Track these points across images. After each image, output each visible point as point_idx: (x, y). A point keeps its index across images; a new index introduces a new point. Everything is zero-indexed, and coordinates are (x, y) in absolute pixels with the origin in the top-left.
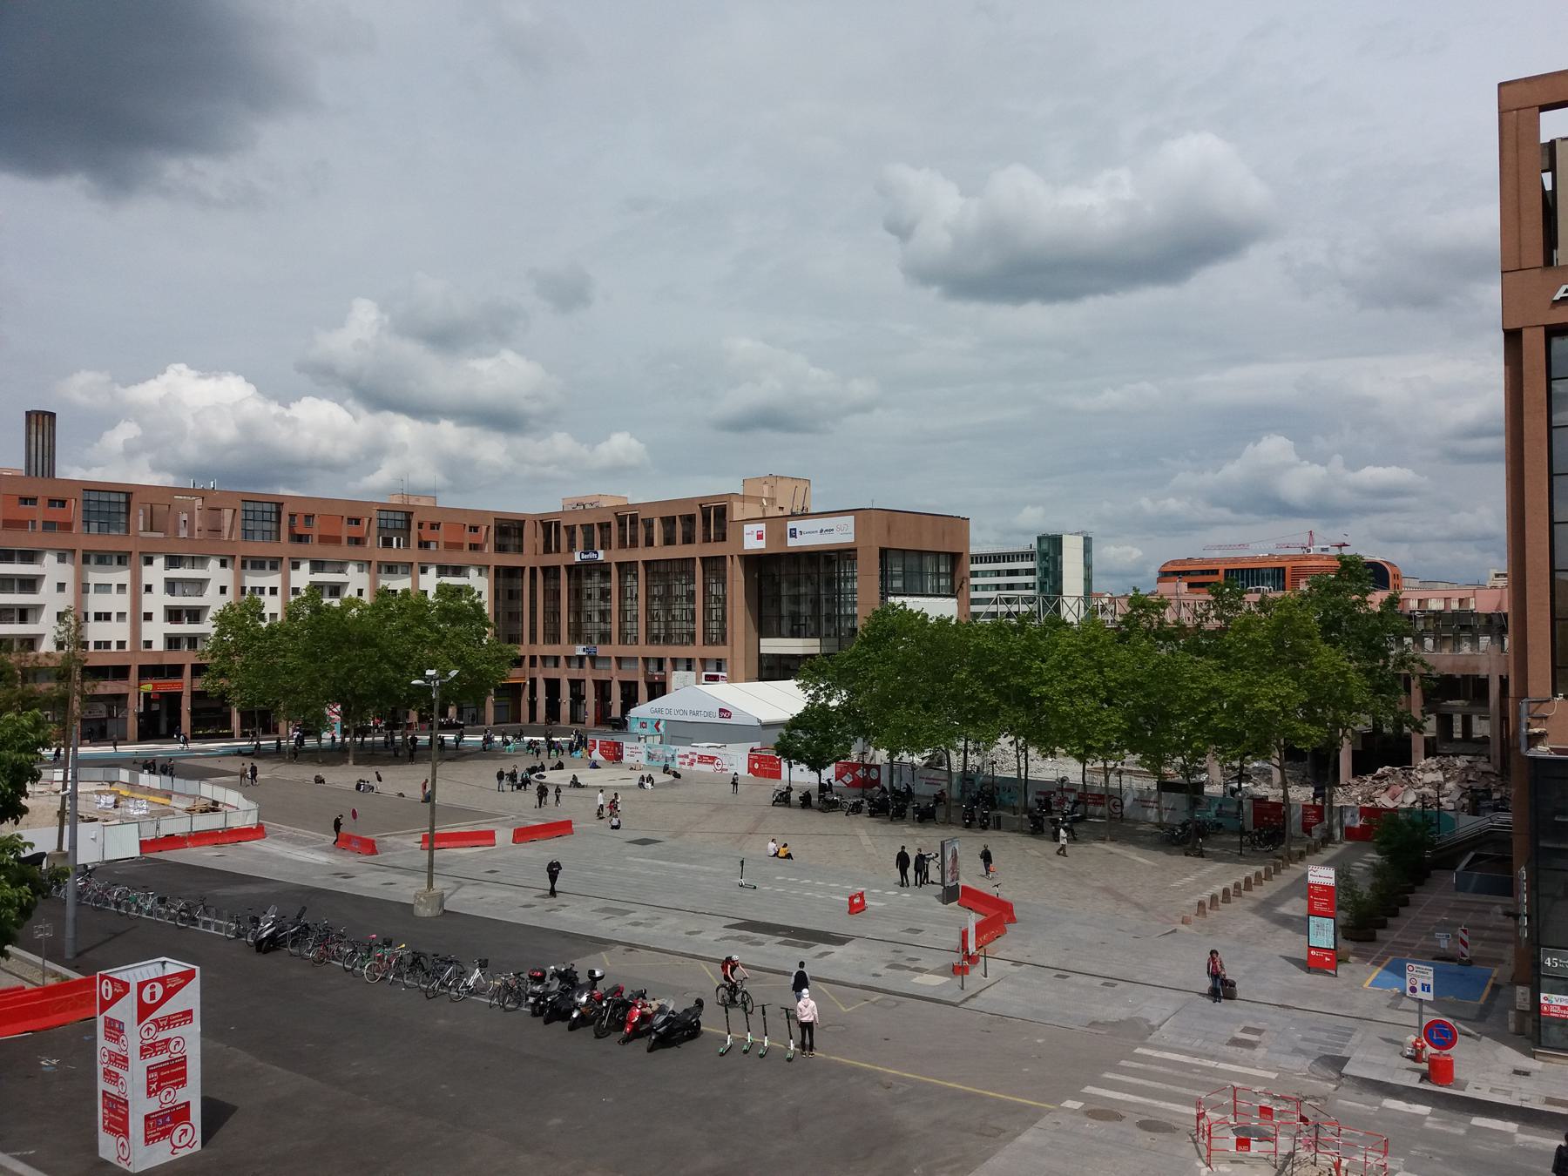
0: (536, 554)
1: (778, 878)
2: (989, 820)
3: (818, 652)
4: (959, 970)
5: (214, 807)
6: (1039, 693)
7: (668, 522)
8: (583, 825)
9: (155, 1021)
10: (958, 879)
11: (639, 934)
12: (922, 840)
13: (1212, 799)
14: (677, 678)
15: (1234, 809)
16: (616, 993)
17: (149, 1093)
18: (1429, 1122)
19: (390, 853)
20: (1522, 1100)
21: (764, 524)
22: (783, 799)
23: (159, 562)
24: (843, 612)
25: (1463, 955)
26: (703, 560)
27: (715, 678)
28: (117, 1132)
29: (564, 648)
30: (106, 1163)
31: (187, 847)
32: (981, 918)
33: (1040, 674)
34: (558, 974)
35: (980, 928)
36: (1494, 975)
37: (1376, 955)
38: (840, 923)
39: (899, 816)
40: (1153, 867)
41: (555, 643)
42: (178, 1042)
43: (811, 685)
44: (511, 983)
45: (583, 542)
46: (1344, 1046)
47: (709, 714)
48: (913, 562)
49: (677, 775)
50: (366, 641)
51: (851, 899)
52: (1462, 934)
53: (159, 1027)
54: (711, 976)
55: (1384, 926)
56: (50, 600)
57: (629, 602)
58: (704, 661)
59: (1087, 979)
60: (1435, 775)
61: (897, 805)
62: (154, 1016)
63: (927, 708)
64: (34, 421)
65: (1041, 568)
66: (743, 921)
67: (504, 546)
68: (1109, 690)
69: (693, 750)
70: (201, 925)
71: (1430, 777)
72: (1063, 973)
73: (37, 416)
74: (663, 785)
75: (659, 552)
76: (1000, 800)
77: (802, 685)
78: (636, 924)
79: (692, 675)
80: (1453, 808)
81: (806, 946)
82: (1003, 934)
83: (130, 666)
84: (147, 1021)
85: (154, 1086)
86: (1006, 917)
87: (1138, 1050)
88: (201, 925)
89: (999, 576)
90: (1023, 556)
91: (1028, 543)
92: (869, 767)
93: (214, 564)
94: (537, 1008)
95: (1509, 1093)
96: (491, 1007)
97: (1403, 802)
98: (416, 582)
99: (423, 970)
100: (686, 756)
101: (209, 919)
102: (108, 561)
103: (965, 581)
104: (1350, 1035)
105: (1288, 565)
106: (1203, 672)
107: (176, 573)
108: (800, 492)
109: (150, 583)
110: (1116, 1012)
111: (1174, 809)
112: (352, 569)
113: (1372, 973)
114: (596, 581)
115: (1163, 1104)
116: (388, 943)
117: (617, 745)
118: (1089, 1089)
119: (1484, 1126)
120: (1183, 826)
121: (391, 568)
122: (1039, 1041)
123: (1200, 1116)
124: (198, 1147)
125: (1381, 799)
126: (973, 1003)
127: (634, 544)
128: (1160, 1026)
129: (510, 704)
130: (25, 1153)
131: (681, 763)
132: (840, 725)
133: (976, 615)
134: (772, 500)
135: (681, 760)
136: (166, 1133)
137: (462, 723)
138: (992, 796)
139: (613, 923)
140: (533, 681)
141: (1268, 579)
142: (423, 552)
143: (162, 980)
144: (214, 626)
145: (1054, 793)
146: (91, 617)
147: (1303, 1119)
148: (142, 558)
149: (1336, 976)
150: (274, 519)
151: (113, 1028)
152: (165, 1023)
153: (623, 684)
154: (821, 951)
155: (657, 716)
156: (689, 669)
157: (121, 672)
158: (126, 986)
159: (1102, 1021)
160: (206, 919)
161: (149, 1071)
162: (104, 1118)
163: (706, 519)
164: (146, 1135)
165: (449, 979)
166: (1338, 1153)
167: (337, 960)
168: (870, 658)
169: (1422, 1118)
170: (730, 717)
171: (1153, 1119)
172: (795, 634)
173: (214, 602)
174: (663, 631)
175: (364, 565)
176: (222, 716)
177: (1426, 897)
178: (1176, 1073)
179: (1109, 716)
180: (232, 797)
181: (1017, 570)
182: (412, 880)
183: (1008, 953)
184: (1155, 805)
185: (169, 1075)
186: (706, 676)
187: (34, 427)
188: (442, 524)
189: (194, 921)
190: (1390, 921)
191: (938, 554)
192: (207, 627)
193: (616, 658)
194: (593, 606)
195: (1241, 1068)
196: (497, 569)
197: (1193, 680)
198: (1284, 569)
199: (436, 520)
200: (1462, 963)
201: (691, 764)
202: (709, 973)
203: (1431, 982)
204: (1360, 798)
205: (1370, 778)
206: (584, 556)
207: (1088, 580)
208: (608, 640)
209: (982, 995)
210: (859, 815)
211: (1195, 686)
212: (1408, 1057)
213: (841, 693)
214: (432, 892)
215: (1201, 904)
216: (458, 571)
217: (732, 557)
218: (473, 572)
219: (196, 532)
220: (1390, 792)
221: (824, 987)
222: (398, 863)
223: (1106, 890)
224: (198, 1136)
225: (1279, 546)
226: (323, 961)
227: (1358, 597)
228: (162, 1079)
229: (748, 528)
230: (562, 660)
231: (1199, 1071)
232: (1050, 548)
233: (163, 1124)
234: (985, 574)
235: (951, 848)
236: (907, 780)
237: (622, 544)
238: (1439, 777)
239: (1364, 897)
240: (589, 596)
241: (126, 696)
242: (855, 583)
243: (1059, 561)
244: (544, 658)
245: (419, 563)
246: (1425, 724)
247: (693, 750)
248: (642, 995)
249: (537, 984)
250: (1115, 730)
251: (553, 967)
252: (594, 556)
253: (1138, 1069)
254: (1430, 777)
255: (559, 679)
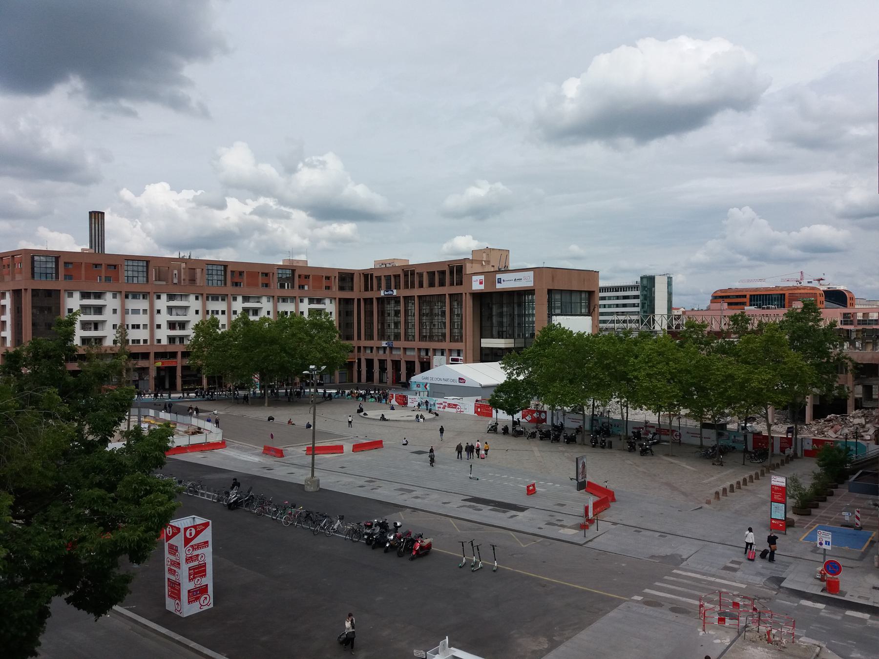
0: (360, 291)
1: (490, 474)
2: (605, 443)
3: (513, 346)
4: (583, 527)
5: (198, 431)
6: (633, 376)
7: (431, 274)
8: (388, 442)
9: (192, 546)
10: (585, 477)
11: (418, 503)
12: (568, 454)
13: (731, 432)
14: (437, 359)
15: (742, 438)
16: (407, 534)
17: (190, 580)
18: (823, 612)
19: (290, 457)
20: (874, 603)
21: (483, 276)
22: (493, 429)
23: (164, 297)
24: (527, 313)
25: (857, 524)
26: (450, 295)
27: (457, 360)
28: (175, 598)
29: (374, 343)
30: (170, 612)
31: (187, 452)
32: (597, 499)
33: (633, 365)
34: (378, 524)
35: (595, 505)
36: (873, 535)
37: (810, 523)
38: (521, 500)
39: (556, 439)
40: (694, 471)
41: (370, 340)
42: (202, 556)
43: (508, 368)
44: (355, 528)
45: (385, 284)
46: (784, 572)
47: (453, 381)
48: (566, 298)
49: (437, 415)
50: (273, 341)
51: (528, 487)
52: (857, 513)
53: (194, 549)
54: (455, 526)
55: (817, 507)
56: (110, 318)
57: (410, 318)
58: (450, 351)
59: (652, 533)
60: (860, 420)
61: (555, 434)
62: (192, 543)
63: (571, 382)
64: (93, 217)
65: (642, 295)
66: (471, 497)
67: (343, 287)
68: (671, 373)
69: (445, 400)
70: (200, 495)
71: (857, 421)
72: (638, 529)
73: (95, 214)
74: (430, 420)
75: (426, 291)
76: (613, 432)
77: (504, 367)
78: (417, 497)
79: (444, 358)
80: (869, 438)
81: (504, 512)
82: (609, 508)
83: (150, 353)
84: (188, 546)
85: (192, 577)
86: (610, 498)
87: (675, 571)
88: (200, 495)
89: (618, 299)
90: (632, 288)
91: (632, 279)
92: (540, 412)
93: (192, 298)
94: (369, 542)
95: (868, 599)
96: (345, 540)
97: (841, 435)
98: (297, 307)
99: (312, 520)
100: (441, 404)
101: (204, 492)
102: (137, 298)
103: (596, 306)
104: (788, 566)
105: (787, 293)
106: (722, 365)
107: (172, 303)
108: (504, 257)
109: (159, 309)
110: (666, 551)
111: (710, 438)
112: (264, 300)
113: (805, 533)
114: (393, 306)
115: (684, 599)
116: (294, 506)
117: (405, 397)
118: (647, 591)
119: (852, 615)
120: (713, 448)
121: (284, 300)
122: (623, 565)
123: (701, 606)
124: (212, 606)
125: (828, 433)
126: (590, 545)
127: (413, 286)
128: (687, 559)
129: (348, 372)
130: (131, 607)
131: (439, 407)
132: (525, 390)
133: (601, 330)
134: (488, 262)
135: (438, 406)
136: (198, 599)
137: (322, 382)
138: (608, 430)
139: (405, 497)
140: (359, 360)
141: (775, 301)
142: (301, 291)
143: (195, 527)
144: (193, 333)
145: (643, 428)
146: (130, 327)
147: (755, 609)
148: (155, 296)
149: (785, 534)
150: (223, 274)
151: (173, 549)
152: (196, 547)
153: (407, 362)
154: (512, 515)
155: (426, 381)
156: (442, 354)
157: (145, 356)
158: (178, 529)
159: (657, 555)
160: (202, 491)
161: (190, 570)
162: (168, 591)
163: (452, 273)
164: (189, 600)
165: (325, 525)
166: (771, 627)
167: (268, 514)
168: (540, 353)
169: (820, 610)
170: (464, 383)
171: (678, 606)
172: (500, 336)
173: (194, 319)
174: (428, 334)
175: (271, 297)
176: (197, 379)
177: (843, 491)
178: (693, 583)
179: (671, 389)
180: (209, 426)
181: (623, 307)
182: (302, 471)
183: (611, 518)
184: (699, 436)
185: (198, 571)
186: (452, 359)
187: (93, 220)
188: (311, 276)
189: (196, 492)
190: (821, 504)
191: (581, 292)
192: (189, 332)
193: (403, 348)
194: (391, 319)
195: (727, 582)
196: (340, 299)
197: (718, 370)
198: (784, 294)
199: (307, 274)
200: (856, 529)
201: (444, 408)
202: (454, 525)
203: (830, 540)
204: (816, 432)
205: (823, 421)
206: (386, 293)
207: (670, 301)
208: (399, 339)
209: (595, 540)
210: (534, 439)
211: (719, 373)
212: (818, 579)
213: (525, 372)
214: (314, 479)
215: (717, 493)
216: (319, 301)
217: (466, 294)
218: (327, 301)
219: (182, 281)
220: (833, 429)
221: (513, 533)
222: (295, 462)
223: (668, 484)
224: (212, 601)
225: (783, 280)
226: (261, 515)
227: (813, 323)
228: (195, 573)
229: (474, 278)
230: (375, 348)
231: (705, 583)
232: (648, 283)
233: (197, 594)
234: (610, 298)
235: (582, 462)
236: (561, 420)
237: (406, 287)
238: (862, 421)
239: (807, 491)
240: (389, 315)
241: (148, 368)
242: (534, 318)
243: (653, 291)
244: (365, 348)
245: (299, 297)
246: (849, 395)
247: (445, 400)
248: (421, 536)
249: (368, 529)
250: (675, 396)
251: (376, 520)
252: (391, 292)
253: (673, 581)
254: (857, 421)
255: (373, 359)
